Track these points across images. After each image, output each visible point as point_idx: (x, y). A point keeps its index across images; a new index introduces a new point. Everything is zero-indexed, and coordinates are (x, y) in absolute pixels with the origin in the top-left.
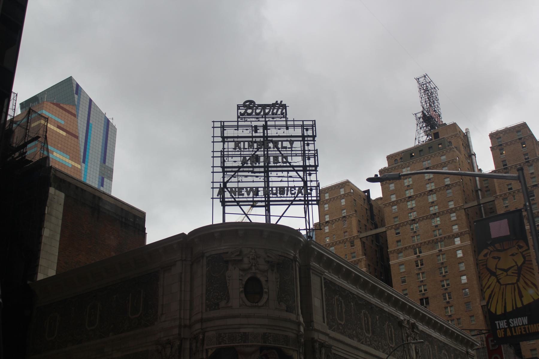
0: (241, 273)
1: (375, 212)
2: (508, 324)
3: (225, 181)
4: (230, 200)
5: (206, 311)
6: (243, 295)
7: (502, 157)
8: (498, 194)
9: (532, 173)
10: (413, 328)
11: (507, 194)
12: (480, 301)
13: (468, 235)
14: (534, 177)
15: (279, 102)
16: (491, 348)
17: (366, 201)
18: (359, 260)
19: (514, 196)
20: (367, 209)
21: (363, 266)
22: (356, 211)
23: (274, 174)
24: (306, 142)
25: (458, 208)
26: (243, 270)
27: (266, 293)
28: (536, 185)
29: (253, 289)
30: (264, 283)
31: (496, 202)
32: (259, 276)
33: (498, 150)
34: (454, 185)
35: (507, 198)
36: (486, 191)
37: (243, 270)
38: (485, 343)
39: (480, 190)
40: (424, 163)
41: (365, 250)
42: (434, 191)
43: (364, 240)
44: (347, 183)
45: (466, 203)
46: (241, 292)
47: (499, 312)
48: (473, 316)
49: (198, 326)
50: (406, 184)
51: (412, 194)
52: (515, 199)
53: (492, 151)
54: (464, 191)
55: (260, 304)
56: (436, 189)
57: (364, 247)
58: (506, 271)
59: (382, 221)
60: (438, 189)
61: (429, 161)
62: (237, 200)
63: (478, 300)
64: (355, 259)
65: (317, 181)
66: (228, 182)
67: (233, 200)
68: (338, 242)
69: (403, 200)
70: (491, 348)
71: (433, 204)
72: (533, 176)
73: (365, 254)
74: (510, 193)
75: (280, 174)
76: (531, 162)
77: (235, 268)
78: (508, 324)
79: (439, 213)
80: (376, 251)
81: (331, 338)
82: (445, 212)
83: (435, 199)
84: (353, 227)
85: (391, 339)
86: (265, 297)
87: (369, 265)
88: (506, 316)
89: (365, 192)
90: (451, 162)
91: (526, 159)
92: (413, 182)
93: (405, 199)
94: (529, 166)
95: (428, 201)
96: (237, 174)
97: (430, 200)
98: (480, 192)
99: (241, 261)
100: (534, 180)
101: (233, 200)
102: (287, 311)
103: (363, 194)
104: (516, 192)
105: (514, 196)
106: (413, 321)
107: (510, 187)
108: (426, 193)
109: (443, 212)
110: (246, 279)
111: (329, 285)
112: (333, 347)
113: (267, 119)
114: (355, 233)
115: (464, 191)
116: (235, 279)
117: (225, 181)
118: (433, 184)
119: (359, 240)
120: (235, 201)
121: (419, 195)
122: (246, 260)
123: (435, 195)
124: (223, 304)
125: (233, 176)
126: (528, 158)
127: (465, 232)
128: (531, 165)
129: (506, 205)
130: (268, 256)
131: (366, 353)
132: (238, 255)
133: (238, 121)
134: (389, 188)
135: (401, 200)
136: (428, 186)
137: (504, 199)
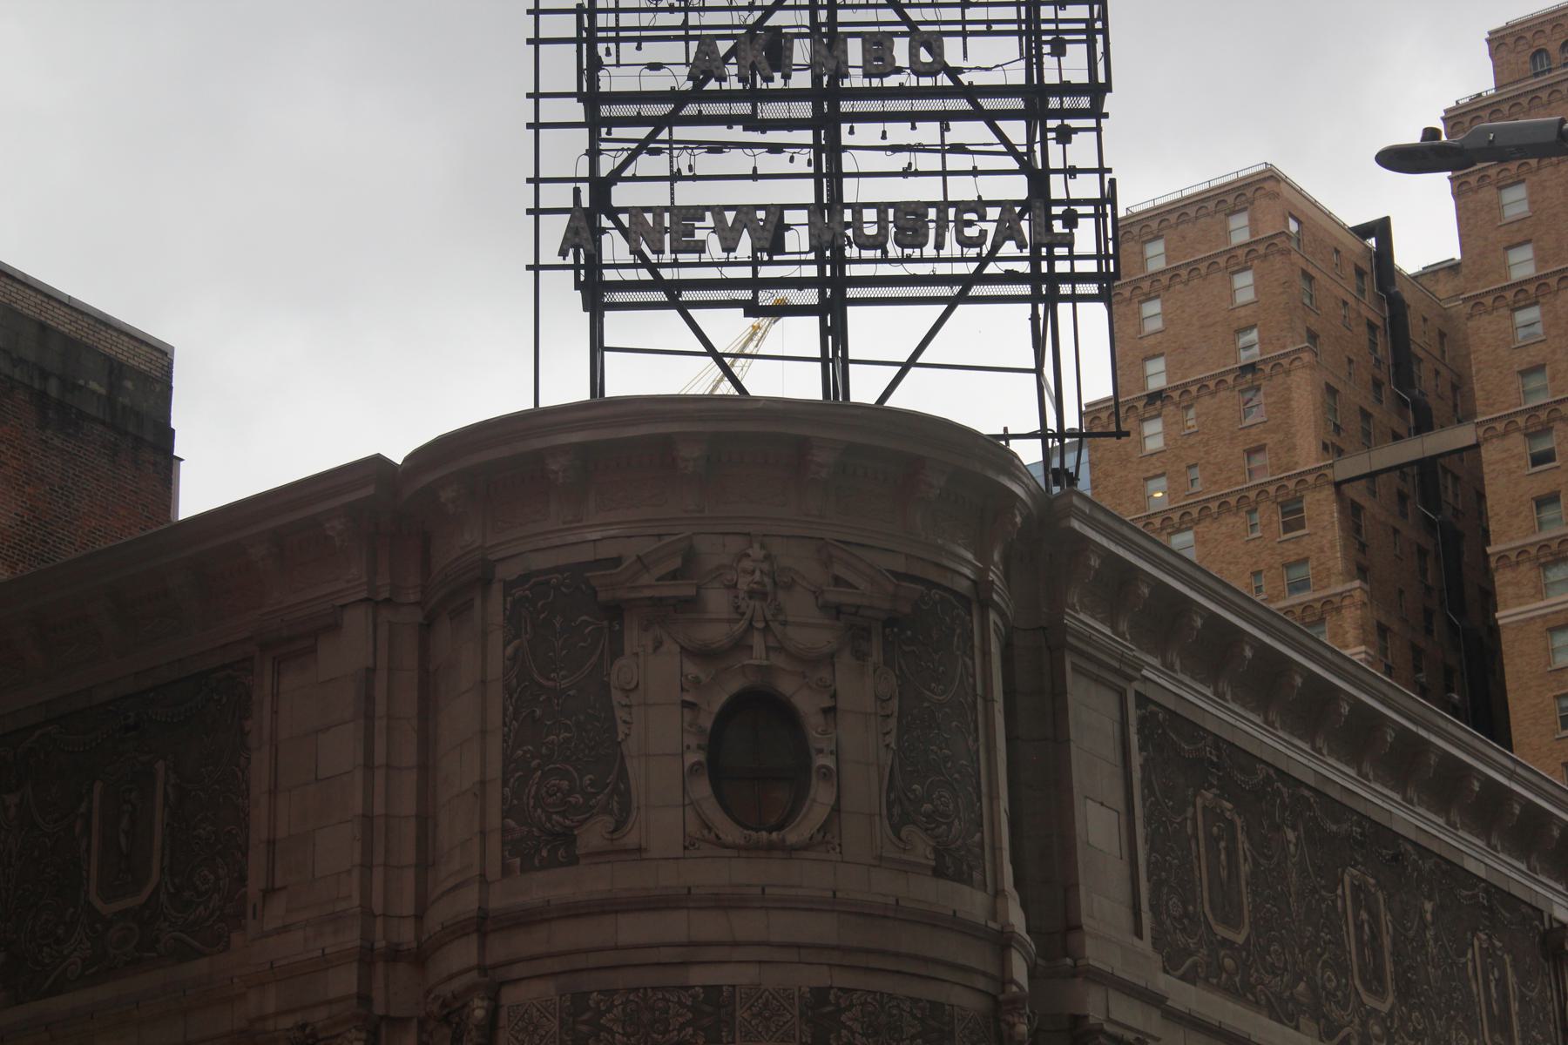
0: (691, 669)
4: (630, 275)
5: (506, 871)
6: (702, 789)
17: (1371, 284)
18: (1327, 601)
20: (1371, 327)
22: (1313, 337)
23: (867, 133)
26: (704, 654)
27: (826, 774)
29: (756, 751)
32: (786, 686)
37: (704, 654)
41: (1363, 547)
43: (1355, 492)
44: (1268, 186)
46: (695, 769)
49: (462, 954)
59: (1455, 388)
62: (666, 274)
65: (1102, 171)
66: (616, 176)
67: (644, 275)
68: (1214, 506)
73: (1362, 572)
75: (899, 133)
80: (1422, 552)
86: (822, 795)
87: (1383, 630)
89: (1363, 231)
96: (664, 135)
99: (690, 605)
101: (644, 275)
102: (938, 872)
103: (1352, 242)
110: (719, 699)
114: (1308, 455)
116: (659, 715)
119: (1328, 492)
122: (717, 601)
124: (593, 835)
125: (643, 146)
130: (838, 581)
132: (674, 575)
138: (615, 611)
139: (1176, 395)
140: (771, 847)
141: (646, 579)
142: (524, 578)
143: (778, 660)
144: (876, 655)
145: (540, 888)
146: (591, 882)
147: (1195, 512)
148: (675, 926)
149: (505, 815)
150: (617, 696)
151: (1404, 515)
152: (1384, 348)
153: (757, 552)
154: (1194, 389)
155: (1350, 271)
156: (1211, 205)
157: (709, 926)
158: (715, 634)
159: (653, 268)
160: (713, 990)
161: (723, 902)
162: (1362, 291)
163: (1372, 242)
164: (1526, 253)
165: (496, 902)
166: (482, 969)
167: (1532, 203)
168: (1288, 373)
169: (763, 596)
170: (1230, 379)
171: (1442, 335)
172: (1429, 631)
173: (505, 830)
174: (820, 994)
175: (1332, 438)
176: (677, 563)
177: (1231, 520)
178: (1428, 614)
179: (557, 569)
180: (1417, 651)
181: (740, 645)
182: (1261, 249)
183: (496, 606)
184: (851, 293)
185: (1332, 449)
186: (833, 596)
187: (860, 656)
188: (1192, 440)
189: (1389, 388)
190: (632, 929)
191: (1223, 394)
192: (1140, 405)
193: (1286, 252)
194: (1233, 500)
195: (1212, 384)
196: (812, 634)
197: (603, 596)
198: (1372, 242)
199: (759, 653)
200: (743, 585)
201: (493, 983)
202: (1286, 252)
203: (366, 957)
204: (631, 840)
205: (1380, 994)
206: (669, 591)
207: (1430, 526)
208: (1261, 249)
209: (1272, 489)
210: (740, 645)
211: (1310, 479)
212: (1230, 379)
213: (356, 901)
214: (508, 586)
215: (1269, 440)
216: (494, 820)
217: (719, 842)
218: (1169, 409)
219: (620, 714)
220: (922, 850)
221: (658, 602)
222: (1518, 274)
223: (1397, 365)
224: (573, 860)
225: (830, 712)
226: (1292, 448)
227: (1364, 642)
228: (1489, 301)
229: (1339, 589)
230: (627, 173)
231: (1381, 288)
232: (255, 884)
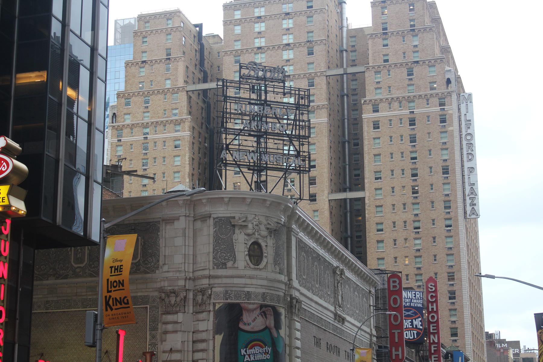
0: (246, 237)
1: (206, 53)
3: (228, 143)
4: (232, 162)
5: (214, 268)
6: (247, 258)
7: (384, 17)
8: (370, 65)
9: (416, 46)
11: (382, 67)
12: (329, 194)
13: (325, 110)
14: (417, 52)
15: (280, 67)
16: (392, 289)
18: (182, 120)
19: (389, 71)
20: (196, 51)
22: (184, 53)
23: (271, 141)
24: (301, 112)
25: (319, 74)
26: (248, 235)
27: (266, 257)
28: (417, 62)
29: (256, 253)
30: (264, 247)
31: (367, 75)
32: (260, 241)
33: (379, 8)
34: (319, 42)
35: (380, 72)
36: (351, 51)
37: (248, 235)
39: (346, 51)
40: (284, 6)
41: (191, 107)
42: (292, 45)
43: (190, 93)
44: (178, 14)
45: (329, 68)
46: (246, 255)
48: (317, 211)
49: (206, 281)
50: (257, 30)
51: (263, 44)
53: (372, 7)
54: (328, 52)
55: (261, 266)
56: (295, 44)
57: (190, 102)
59: (211, 66)
61: (291, 5)
62: (238, 163)
63: (326, 192)
64: (176, 118)
65: (309, 152)
66: (230, 144)
67: (234, 163)
68: (156, 92)
69: (250, 50)
71: (288, 63)
72: (417, 49)
73: (190, 113)
74: (385, 67)
75: (276, 141)
76: (416, 31)
77: (241, 233)
80: (202, 108)
82: (302, 76)
83: (291, 56)
84: (179, 74)
85: (329, 288)
86: (265, 260)
87: (193, 128)
89: (196, 26)
90: (319, 11)
91: (411, 26)
92: (267, 29)
94: (413, 36)
95: (282, 57)
96: (237, 138)
100: (416, 54)
101: (234, 163)
102: (279, 273)
103: (193, 28)
104: (393, 66)
105: (389, 71)
107: (386, 58)
108: (282, 46)
109: (299, 75)
111: (300, 242)
112: (303, 303)
113: (267, 83)
115: (328, 52)
116: (241, 243)
117: (228, 143)
119: (185, 93)
121: (271, 48)
122: (250, 226)
124: (230, 264)
126: (414, 26)
127: (323, 105)
128: (417, 35)
129: (377, 80)
132: (244, 221)
133: (240, 84)
134: (234, 30)
135: (247, 50)
137: (377, 72)
138: (234, 226)
139: (149, 62)
140: (258, 269)
141: (240, 221)
142: (217, 218)
143: (259, 237)
144: (273, 236)
146: (229, 272)
148: (242, 281)
149: (213, 258)
150: (234, 241)
151: (199, 98)
152: (198, 57)
154: (154, 62)
155: (193, 36)
156: (163, 16)
157: (248, 281)
158: (250, 231)
159: (236, 162)
161: (251, 278)
162: (194, 41)
164: (239, 43)
165: (211, 273)
166: (209, 285)
167: (242, 31)
168: (178, 62)
169: (257, 225)
170: (163, 61)
171: (210, 53)
172: (202, 128)
173: (213, 261)
174: (264, 293)
175: (186, 79)
176: (245, 219)
177: (160, 96)
178: (202, 124)
179: (224, 217)
180: (200, 133)
181: (254, 234)
183: (211, 221)
187: (271, 236)
188: (152, 74)
189: (198, 66)
190: (236, 281)
191: (161, 64)
192: (140, 63)
193: (180, 31)
194: (161, 91)
195: (158, 61)
196: (264, 233)
197: (232, 224)
198: (198, 29)
200: (255, 223)
201: (211, 286)
202: (180, 31)
203: (186, 279)
204: (236, 266)
205: (304, 275)
206: (243, 224)
207: (204, 102)
209: (171, 90)
210: (254, 234)
212: (163, 61)
213: (183, 269)
214: (214, 219)
215: (171, 77)
218: (147, 66)
219: (234, 244)
220: (278, 270)
221: (241, 225)
224: (226, 268)
225: (266, 246)
226: (177, 81)
227: (190, 131)
228: (229, 53)
229: (185, 117)
231: (199, 41)
232: (161, 263)
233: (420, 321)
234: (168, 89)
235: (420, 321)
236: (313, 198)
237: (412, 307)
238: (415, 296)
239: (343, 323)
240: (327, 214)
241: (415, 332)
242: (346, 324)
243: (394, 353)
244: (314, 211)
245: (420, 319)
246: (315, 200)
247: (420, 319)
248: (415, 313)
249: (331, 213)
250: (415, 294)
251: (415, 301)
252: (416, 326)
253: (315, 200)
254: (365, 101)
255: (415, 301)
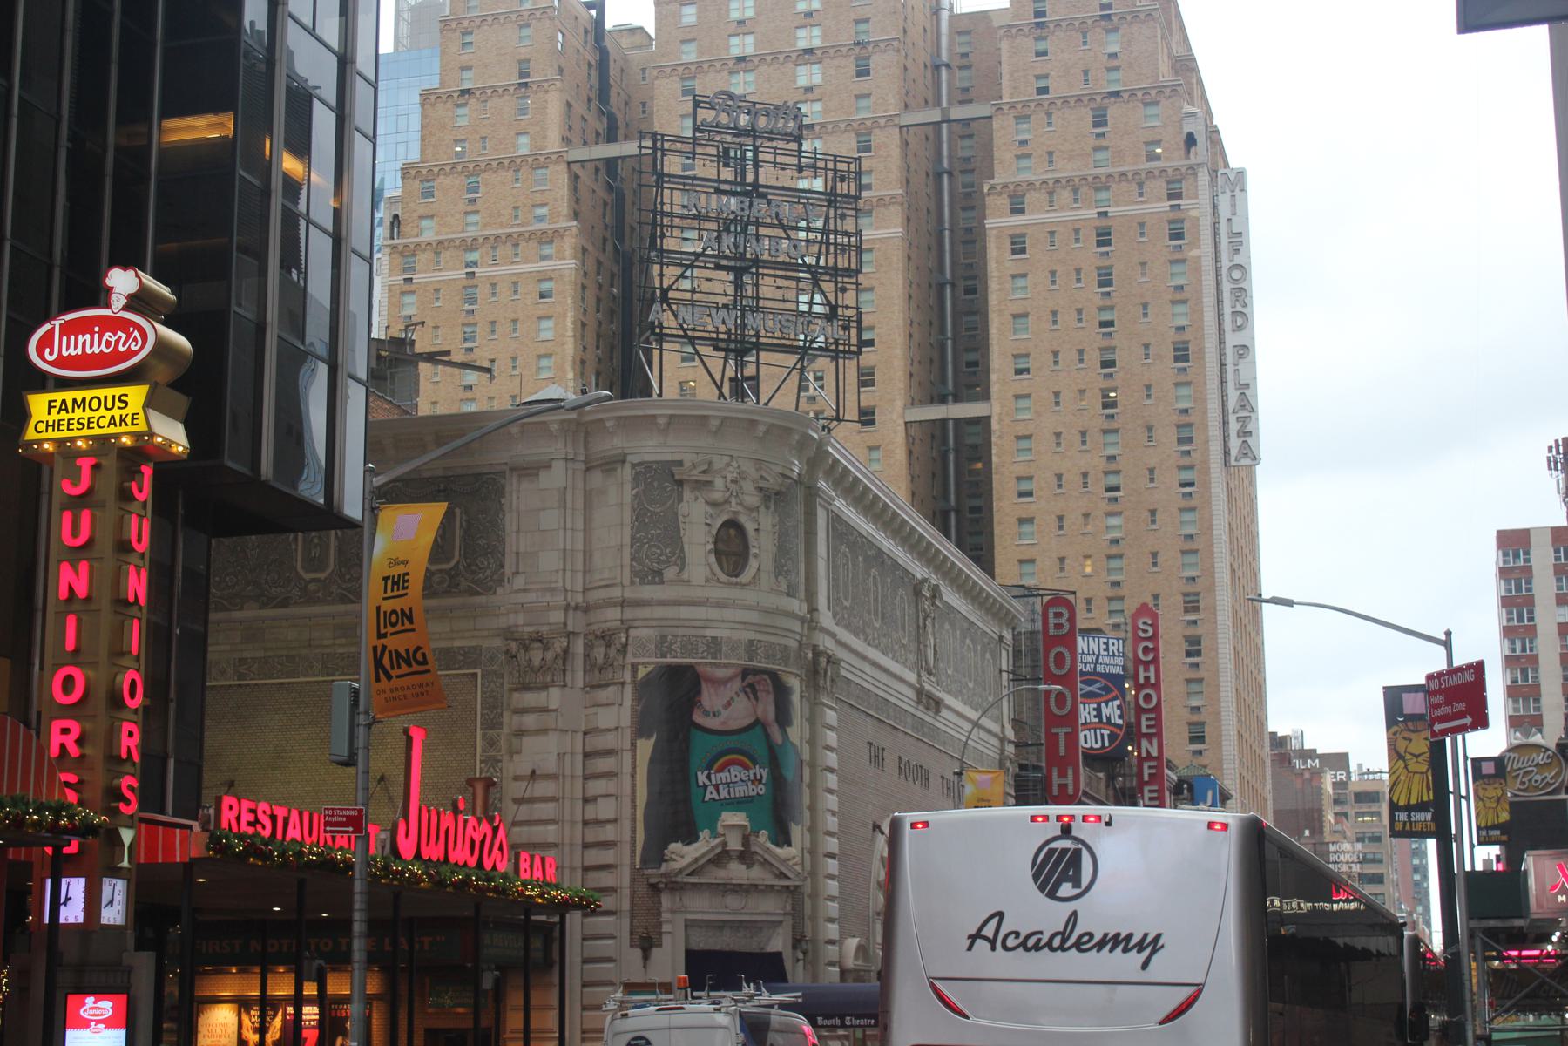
0: (708, 509)
2: (1409, 817)
5: (632, 583)
6: (712, 558)
9: (1113, 56)
10: (934, 597)
11: (1032, 105)
13: (899, 208)
14: (1117, 69)
15: (790, 104)
16: (1052, 631)
17: (591, 38)
19: (1049, 115)
20: (590, 65)
21: (568, 252)
22: (561, 71)
23: (769, 280)
25: (882, 122)
26: (714, 504)
27: (756, 556)
28: (1116, 94)
29: (732, 547)
31: (996, 124)
32: (743, 519)
35: (1028, 117)
37: (714, 504)
38: (1039, 619)
39: (947, 66)
41: (578, 200)
42: (819, 53)
43: (576, 168)
47: (1402, 803)
48: (877, 448)
51: (750, 50)
52: (1050, 124)
54: (906, 69)
55: (744, 578)
56: (825, 50)
57: (575, 189)
58: (1417, 756)
59: (626, 104)
60: (832, 51)
63: (899, 404)
66: (670, 288)
68: (495, 164)
69: (718, 65)
70: (1052, 631)
71: (810, 96)
72: (1115, 63)
73: (576, 215)
74: (1039, 104)
75: (780, 282)
78: (1409, 817)
79: (823, 125)
80: (605, 204)
81: (840, 643)
82: (843, 126)
85: (876, 615)
86: (753, 564)
87: (584, 250)
88: (1409, 808)
92: (758, 14)
93: (724, 63)
94: (1108, 31)
95: (795, 82)
96: (688, 273)
97: (802, 81)
98: (944, 72)
99: (709, 483)
100: (1114, 76)
103: (582, 10)
104: (1059, 103)
105: (1049, 115)
106: (934, 580)
107: (1042, 84)
108: (794, 55)
109: (836, 124)
110: (719, 522)
113: (758, 143)
114: (553, 143)
116: (697, 524)
118: (816, 31)
119: (564, 167)
120: (685, 336)
121: (769, 58)
123: (816, 68)
124: (670, 573)
125: (682, 276)
127: (893, 197)
128: (1115, 30)
130: (762, 477)
131: (874, 664)
132: (704, 472)
136: (801, 33)
137: (1021, 118)
138: (680, 483)
141: (695, 472)
142: (640, 464)
143: (739, 508)
145: (649, 592)
147: (483, 166)
150: (680, 518)
153: (735, 464)
157: (714, 613)
158: (717, 496)
160: (714, 638)
161: (720, 605)
163: (593, 12)
166: (622, 621)
174: (751, 642)
178: (605, 240)
180: (599, 263)
181: (727, 501)
182: (538, 14)
183: (627, 473)
184: (1468, 868)
185: (566, 140)
186: (763, 484)
187: (767, 508)
189: (595, 103)
190: (685, 612)
193: (552, 19)
194: (506, 162)
196: (753, 499)
198: (593, 12)
199: (734, 506)
201: (627, 626)
202: (552, 19)
206: (703, 478)
207: (610, 188)
208: (538, 14)
210: (727, 501)
211: (554, 157)
214: (634, 466)
216: (627, 561)
217: (718, 581)
218: (473, 101)
220: (784, 587)
222: (685, 59)
223: (601, 90)
224: (662, 582)
226: (545, 137)
230: (308, 21)
233: (1119, 707)
234: (524, 158)
235: (1119, 707)
236: (867, 417)
237: (1100, 674)
238: (1107, 650)
239: (937, 711)
240: (900, 454)
241: (1106, 733)
242: (944, 712)
243: (1056, 781)
244: (871, 449)
245: (1117, 702)
246: (872, 422)
247: (1117, 702)
248: (1106, 689)
249: (910, 453)
250: (1106, 644)
251: (1106, 660)
252: (1109, 719)
253: (872, 422)
254: (993, 187)
255: (1106, 660)
